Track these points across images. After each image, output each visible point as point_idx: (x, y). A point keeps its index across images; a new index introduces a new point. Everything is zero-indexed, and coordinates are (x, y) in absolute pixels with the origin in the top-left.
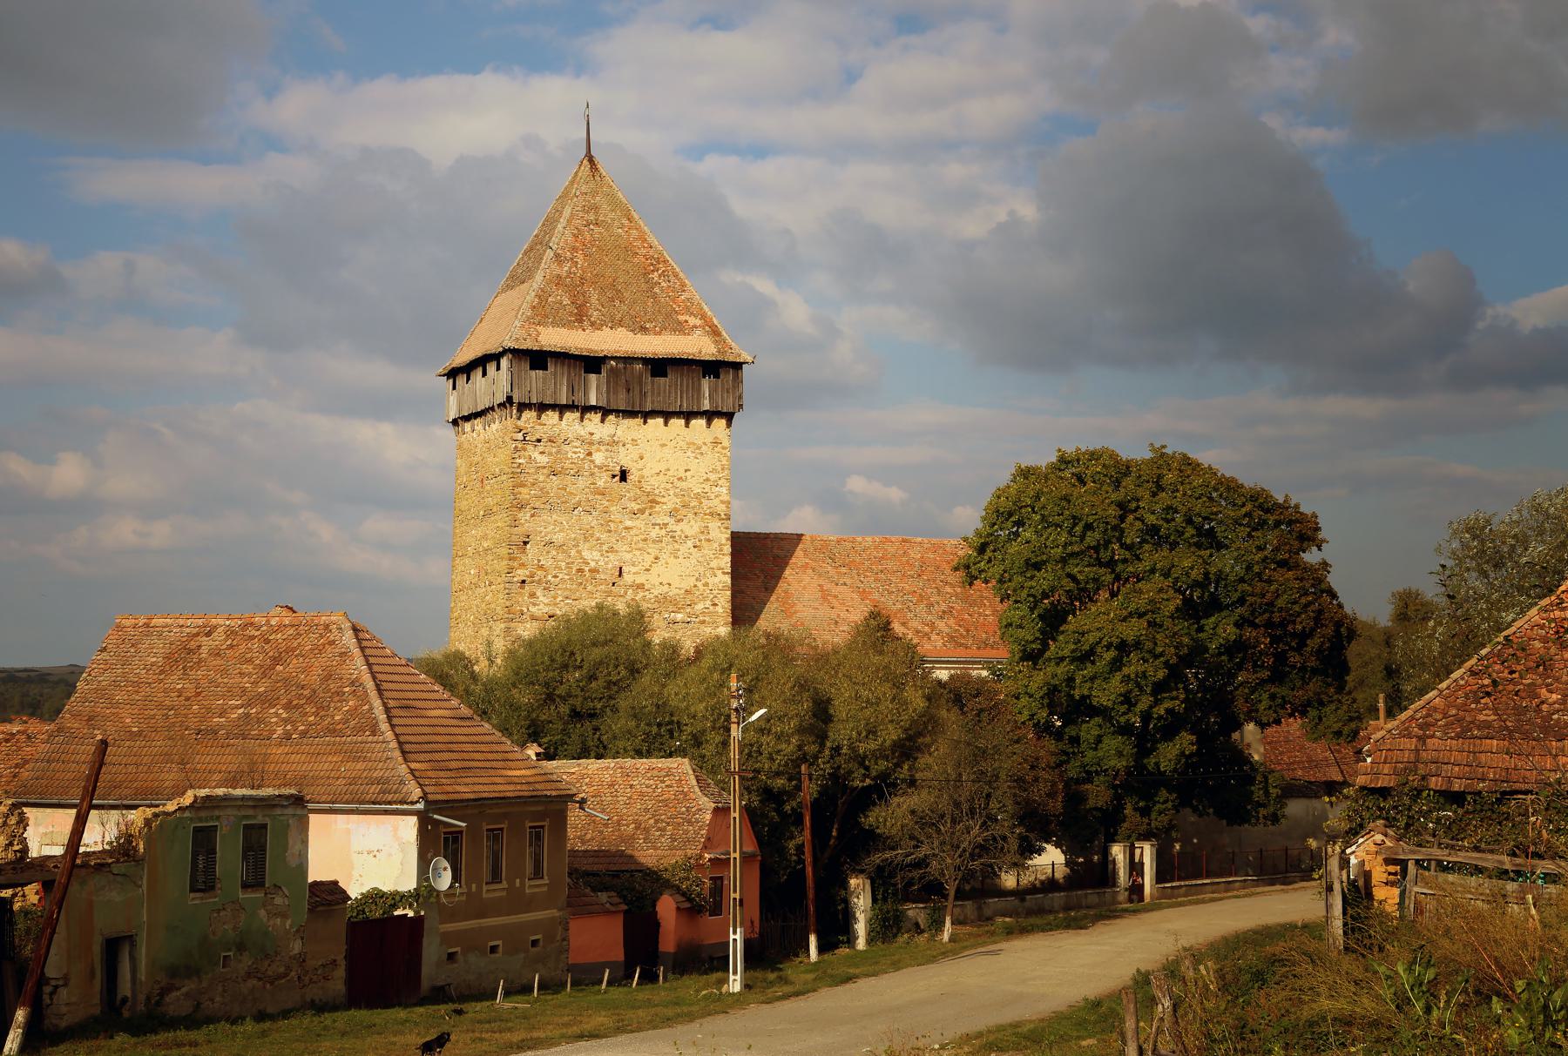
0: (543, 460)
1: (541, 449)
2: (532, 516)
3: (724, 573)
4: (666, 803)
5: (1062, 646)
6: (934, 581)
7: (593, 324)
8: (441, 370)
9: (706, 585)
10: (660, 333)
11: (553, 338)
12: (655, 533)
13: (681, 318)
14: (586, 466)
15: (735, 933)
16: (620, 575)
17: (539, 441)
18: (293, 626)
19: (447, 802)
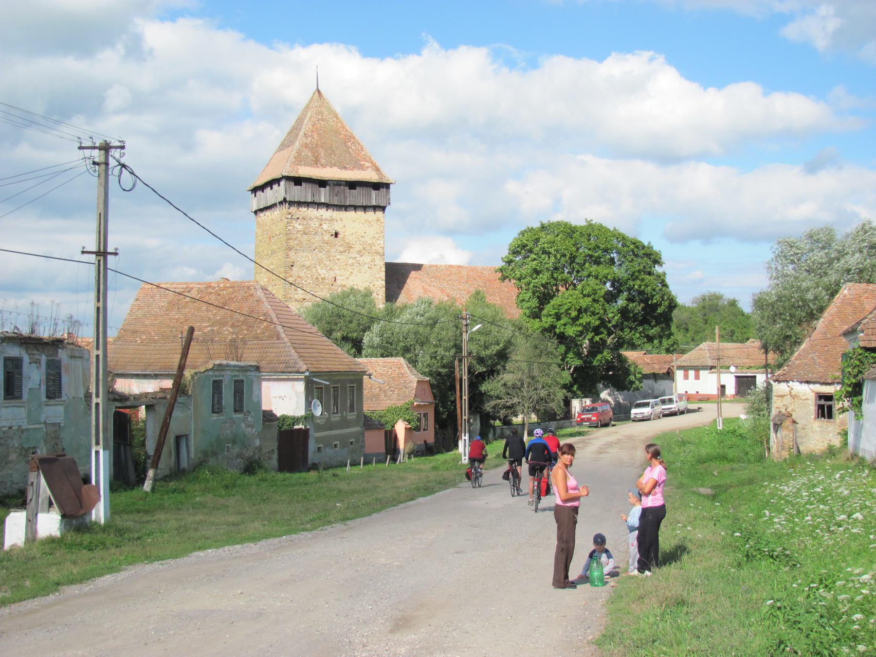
0: (300, 227)
1: (299, 222)
2: (295, 253)
3: (382, 280)
4: (393, 378)
5: (548, 309)
6: (473, 284)
7: (322, 165)
8: (249, 188)
9: (374, 285)
10: (352, 170)
11: (304, 171)
12: (350, 261)
13: (362, 163)
14: (319, 231)
15: (465, 435)
16: (335, 281)
17: (298, 219)
18: (231, 287)
19: (317, 372)
